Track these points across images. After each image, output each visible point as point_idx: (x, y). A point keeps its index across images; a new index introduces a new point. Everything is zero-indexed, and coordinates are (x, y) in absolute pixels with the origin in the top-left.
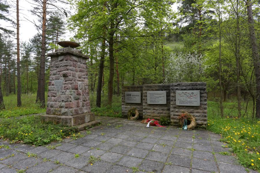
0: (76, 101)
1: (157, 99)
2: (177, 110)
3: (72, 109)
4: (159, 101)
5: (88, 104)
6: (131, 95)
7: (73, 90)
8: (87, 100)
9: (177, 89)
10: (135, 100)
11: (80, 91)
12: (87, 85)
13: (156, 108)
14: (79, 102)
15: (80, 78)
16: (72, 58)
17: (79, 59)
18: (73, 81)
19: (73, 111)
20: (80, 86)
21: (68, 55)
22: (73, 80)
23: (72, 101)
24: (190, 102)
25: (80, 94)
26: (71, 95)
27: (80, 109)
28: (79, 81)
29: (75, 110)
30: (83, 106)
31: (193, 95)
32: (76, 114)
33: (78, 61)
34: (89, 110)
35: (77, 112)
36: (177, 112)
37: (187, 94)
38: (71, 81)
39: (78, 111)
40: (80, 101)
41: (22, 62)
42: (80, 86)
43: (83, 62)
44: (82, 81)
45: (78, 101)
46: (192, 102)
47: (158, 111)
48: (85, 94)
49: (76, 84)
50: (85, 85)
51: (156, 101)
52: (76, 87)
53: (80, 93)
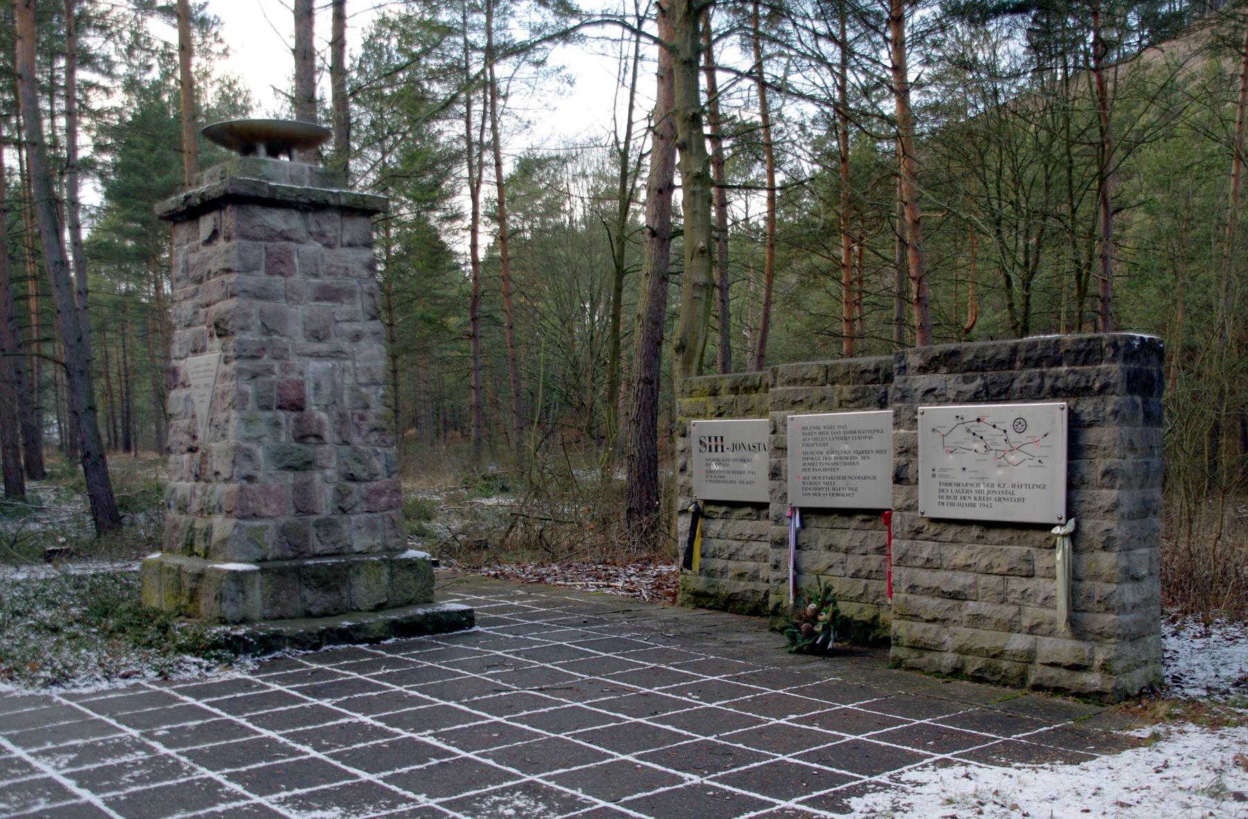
0: (291, 481)
1: (844, 470)
2: (927, 549)
3: (258, 523)
4: (854, 483)
5: (384, 500)
6: (727, 444)
7: (269, 414)
8: (372, 477)
9: (930, 394)
10: (746, 477)
11: (323, 416)
12: (374, 383)
13: (843, 539)
14: (309, 483)
15: (317, 336)
16: (257, 221)
17: (308, 225)
18: (266, 359)
19: (270, 537)
20: (317, 387)
21: (233, 204)
22: (266, 357)
23: (260, 475)
24: (1006, 494)
25: (319, 437)
26: (258, 439)
27: (316, 526)
28: (317, 356)
29: (283, 531)
30: (343, 510)
31: (1023, 438)
32: (291, 554)
33: (302, 233)
34: (388, 533)
35: (298, 542)
36: (929, 565)
37: (987, 431)
38: (254, 357)
39: (306, 535)
40: (317, 477)
41: (512, 179)
42: (317, 387)
43: (347, 238)
44: (337, 354)
45: (301, 477)
46: (1019, 493)
47: (853, 563)
48: (359, 434)
49: (294, 376)
50: (362, 379)
51: (840, 483)
52: (292, 395)
53: (315, 430)
